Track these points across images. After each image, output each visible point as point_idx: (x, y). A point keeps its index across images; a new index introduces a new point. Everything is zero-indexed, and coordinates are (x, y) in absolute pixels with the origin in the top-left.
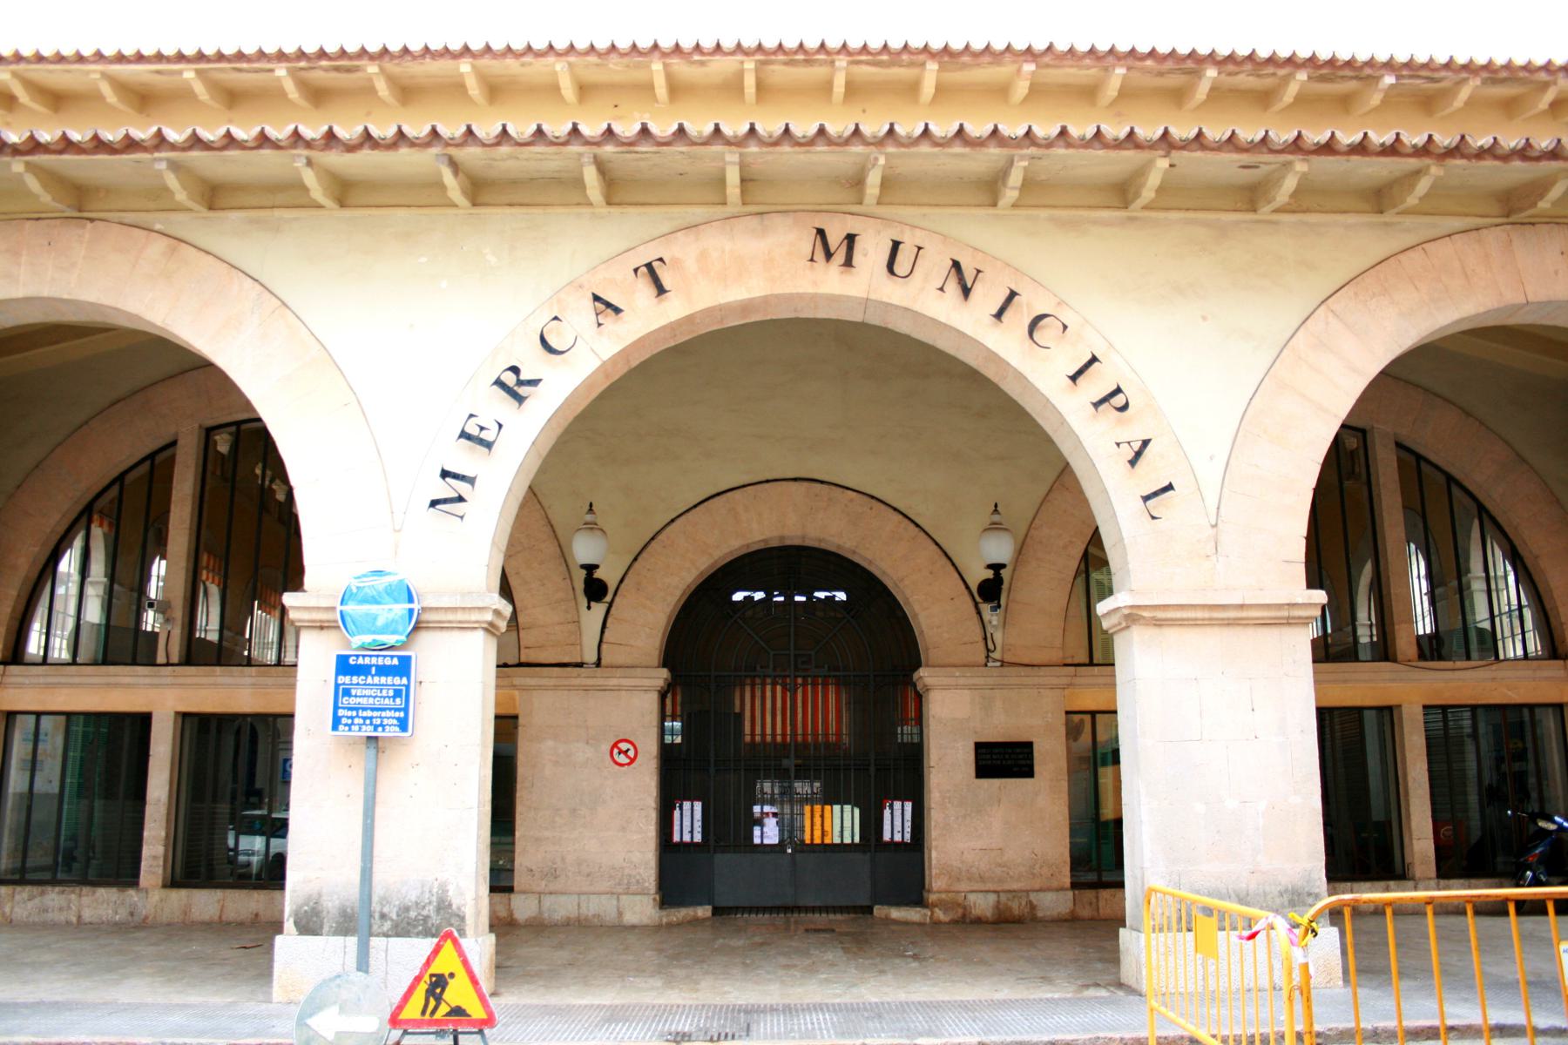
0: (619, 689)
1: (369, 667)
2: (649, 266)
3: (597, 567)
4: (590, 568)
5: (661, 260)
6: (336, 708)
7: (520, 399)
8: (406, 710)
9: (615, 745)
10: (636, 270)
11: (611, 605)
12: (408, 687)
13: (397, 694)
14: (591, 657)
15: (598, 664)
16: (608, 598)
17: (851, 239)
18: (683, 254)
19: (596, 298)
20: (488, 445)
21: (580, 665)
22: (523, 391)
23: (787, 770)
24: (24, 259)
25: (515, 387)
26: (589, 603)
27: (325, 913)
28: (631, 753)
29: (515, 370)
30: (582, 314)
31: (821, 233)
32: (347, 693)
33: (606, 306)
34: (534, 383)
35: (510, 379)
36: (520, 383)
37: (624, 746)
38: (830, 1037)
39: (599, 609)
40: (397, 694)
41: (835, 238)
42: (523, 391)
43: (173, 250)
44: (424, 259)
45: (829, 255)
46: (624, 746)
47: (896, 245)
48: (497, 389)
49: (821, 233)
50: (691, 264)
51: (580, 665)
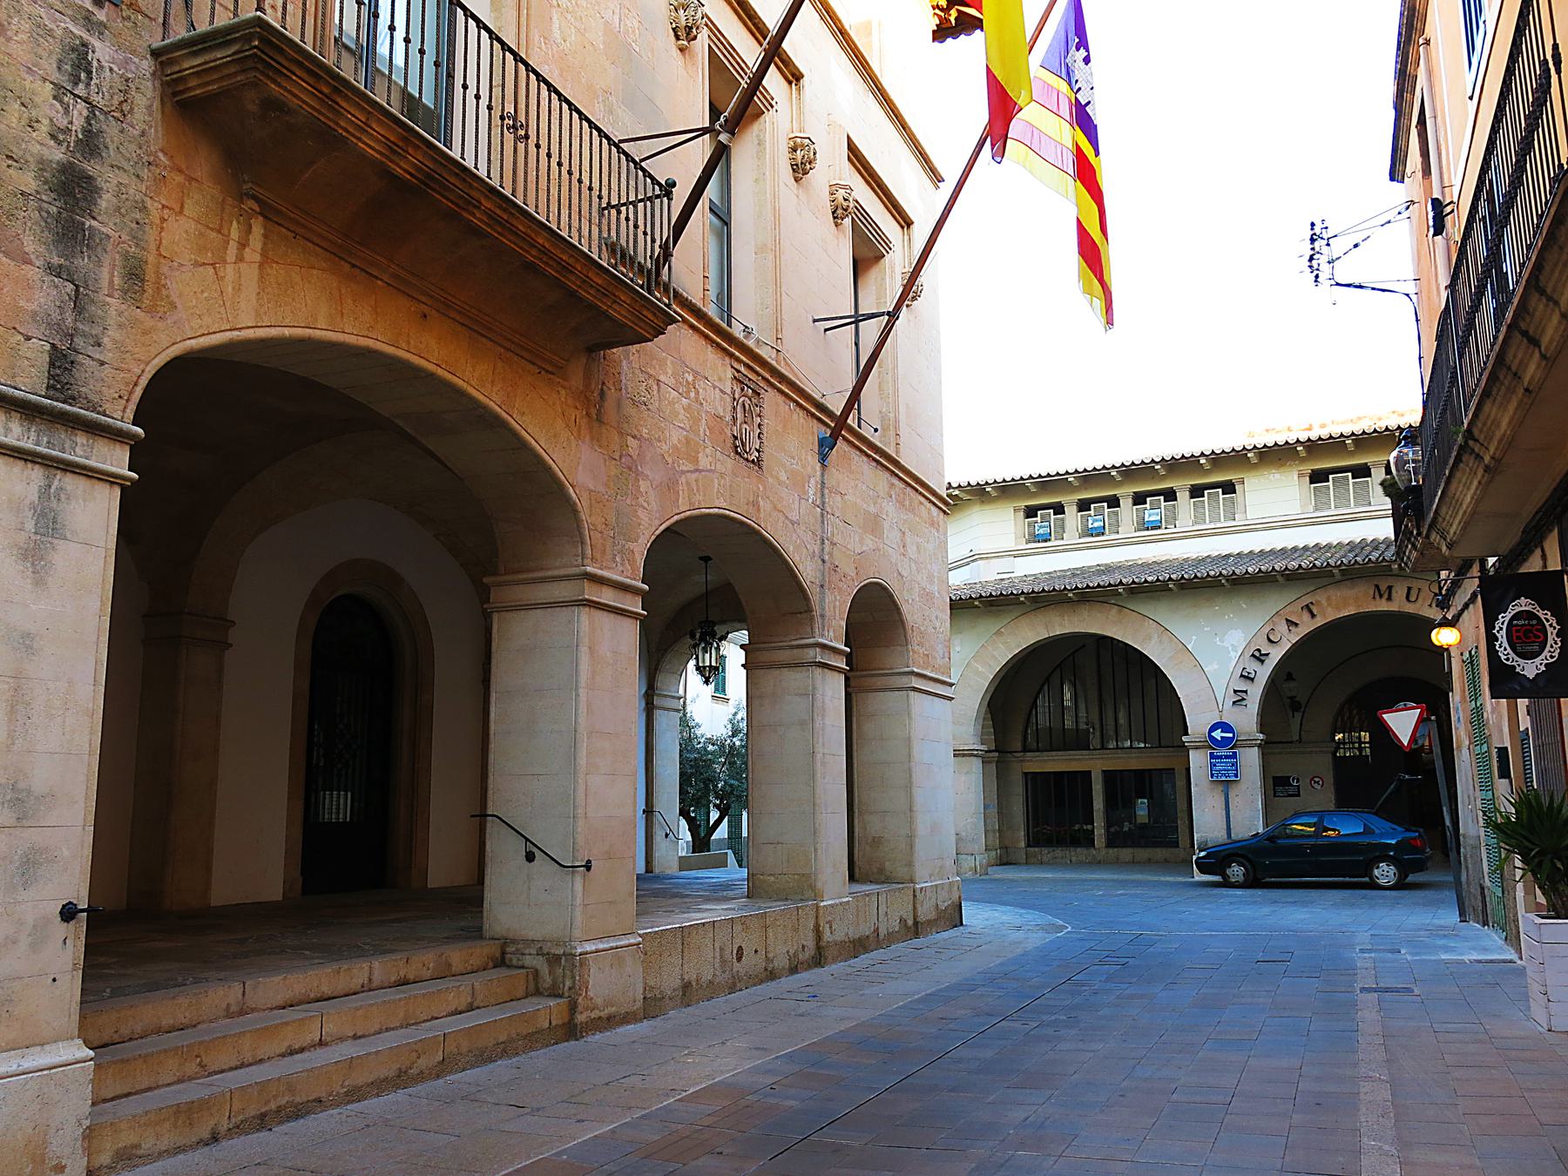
0: (1311, 752)
1: (1222, 756)
2: (1307, 606)
3: (1295, 697)
4: (1292, 698)
5: (1312, 603)
6: (1211, 771)
7: (1262, 662)
8: (1237, 770)
9: (1312, 779)
10: (1302, 608)
11: (1304, 713)
12: (1237, 762)
13: (1233, 765)
14: (1296, 737)
15: (1300, 741)
16: (1302, 710)
17: (1390, 588)
18: (1321, 597)
19: (1287, 620)
20: (1252, 680)
21: (1291, 742)
22: (1262, 658)
23: (1413, 462)
24: (1066, 618)
25: (1260, 657)
26: (1293, 714)
27: (297, 279)
28: (1321, 783)
29: (1259, 650)
30: (1282, 627)
31: (1377, 586)
32: (1215, 765)
33: (1290, 623)
34: (1267, 655)
35: (1257, 654)
36: (1261, 655)
37: (1317, 779)
38: (1480, 786)
39: (1298, 716)
40: (1233, 765)
41: (1383, 588)
42: (1262, 658)
43: (1121, 611)
44: (1217, 608)
45: (1381, 596)
46: (1317, 779)
47: (1409, 589)
48: (1252, 658)
49: (1377, 586)
50: (1324, 602)
51: (1291, 742)
